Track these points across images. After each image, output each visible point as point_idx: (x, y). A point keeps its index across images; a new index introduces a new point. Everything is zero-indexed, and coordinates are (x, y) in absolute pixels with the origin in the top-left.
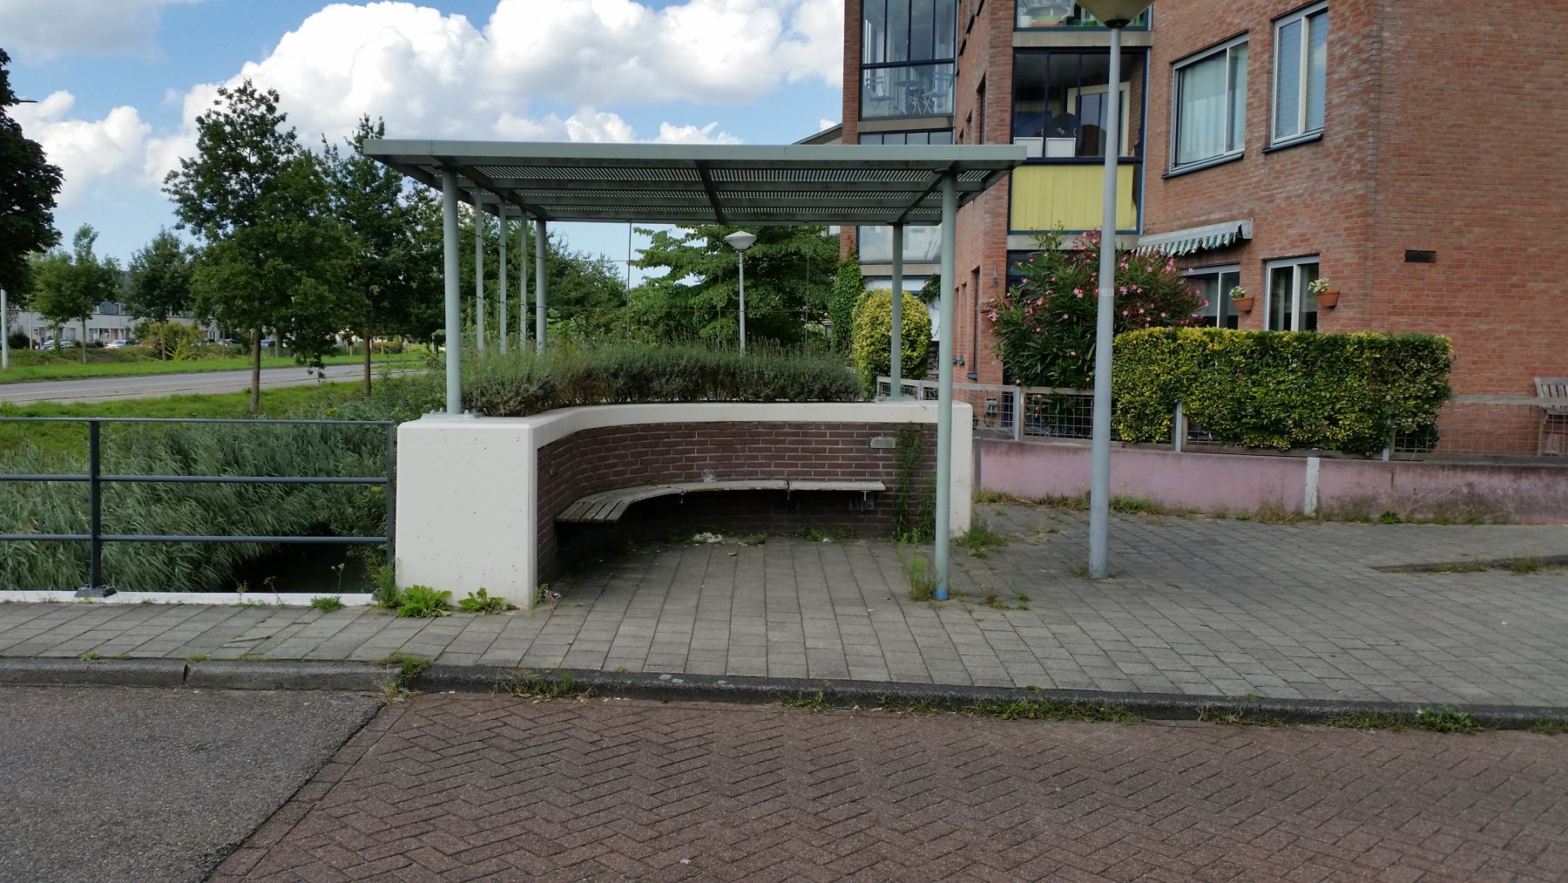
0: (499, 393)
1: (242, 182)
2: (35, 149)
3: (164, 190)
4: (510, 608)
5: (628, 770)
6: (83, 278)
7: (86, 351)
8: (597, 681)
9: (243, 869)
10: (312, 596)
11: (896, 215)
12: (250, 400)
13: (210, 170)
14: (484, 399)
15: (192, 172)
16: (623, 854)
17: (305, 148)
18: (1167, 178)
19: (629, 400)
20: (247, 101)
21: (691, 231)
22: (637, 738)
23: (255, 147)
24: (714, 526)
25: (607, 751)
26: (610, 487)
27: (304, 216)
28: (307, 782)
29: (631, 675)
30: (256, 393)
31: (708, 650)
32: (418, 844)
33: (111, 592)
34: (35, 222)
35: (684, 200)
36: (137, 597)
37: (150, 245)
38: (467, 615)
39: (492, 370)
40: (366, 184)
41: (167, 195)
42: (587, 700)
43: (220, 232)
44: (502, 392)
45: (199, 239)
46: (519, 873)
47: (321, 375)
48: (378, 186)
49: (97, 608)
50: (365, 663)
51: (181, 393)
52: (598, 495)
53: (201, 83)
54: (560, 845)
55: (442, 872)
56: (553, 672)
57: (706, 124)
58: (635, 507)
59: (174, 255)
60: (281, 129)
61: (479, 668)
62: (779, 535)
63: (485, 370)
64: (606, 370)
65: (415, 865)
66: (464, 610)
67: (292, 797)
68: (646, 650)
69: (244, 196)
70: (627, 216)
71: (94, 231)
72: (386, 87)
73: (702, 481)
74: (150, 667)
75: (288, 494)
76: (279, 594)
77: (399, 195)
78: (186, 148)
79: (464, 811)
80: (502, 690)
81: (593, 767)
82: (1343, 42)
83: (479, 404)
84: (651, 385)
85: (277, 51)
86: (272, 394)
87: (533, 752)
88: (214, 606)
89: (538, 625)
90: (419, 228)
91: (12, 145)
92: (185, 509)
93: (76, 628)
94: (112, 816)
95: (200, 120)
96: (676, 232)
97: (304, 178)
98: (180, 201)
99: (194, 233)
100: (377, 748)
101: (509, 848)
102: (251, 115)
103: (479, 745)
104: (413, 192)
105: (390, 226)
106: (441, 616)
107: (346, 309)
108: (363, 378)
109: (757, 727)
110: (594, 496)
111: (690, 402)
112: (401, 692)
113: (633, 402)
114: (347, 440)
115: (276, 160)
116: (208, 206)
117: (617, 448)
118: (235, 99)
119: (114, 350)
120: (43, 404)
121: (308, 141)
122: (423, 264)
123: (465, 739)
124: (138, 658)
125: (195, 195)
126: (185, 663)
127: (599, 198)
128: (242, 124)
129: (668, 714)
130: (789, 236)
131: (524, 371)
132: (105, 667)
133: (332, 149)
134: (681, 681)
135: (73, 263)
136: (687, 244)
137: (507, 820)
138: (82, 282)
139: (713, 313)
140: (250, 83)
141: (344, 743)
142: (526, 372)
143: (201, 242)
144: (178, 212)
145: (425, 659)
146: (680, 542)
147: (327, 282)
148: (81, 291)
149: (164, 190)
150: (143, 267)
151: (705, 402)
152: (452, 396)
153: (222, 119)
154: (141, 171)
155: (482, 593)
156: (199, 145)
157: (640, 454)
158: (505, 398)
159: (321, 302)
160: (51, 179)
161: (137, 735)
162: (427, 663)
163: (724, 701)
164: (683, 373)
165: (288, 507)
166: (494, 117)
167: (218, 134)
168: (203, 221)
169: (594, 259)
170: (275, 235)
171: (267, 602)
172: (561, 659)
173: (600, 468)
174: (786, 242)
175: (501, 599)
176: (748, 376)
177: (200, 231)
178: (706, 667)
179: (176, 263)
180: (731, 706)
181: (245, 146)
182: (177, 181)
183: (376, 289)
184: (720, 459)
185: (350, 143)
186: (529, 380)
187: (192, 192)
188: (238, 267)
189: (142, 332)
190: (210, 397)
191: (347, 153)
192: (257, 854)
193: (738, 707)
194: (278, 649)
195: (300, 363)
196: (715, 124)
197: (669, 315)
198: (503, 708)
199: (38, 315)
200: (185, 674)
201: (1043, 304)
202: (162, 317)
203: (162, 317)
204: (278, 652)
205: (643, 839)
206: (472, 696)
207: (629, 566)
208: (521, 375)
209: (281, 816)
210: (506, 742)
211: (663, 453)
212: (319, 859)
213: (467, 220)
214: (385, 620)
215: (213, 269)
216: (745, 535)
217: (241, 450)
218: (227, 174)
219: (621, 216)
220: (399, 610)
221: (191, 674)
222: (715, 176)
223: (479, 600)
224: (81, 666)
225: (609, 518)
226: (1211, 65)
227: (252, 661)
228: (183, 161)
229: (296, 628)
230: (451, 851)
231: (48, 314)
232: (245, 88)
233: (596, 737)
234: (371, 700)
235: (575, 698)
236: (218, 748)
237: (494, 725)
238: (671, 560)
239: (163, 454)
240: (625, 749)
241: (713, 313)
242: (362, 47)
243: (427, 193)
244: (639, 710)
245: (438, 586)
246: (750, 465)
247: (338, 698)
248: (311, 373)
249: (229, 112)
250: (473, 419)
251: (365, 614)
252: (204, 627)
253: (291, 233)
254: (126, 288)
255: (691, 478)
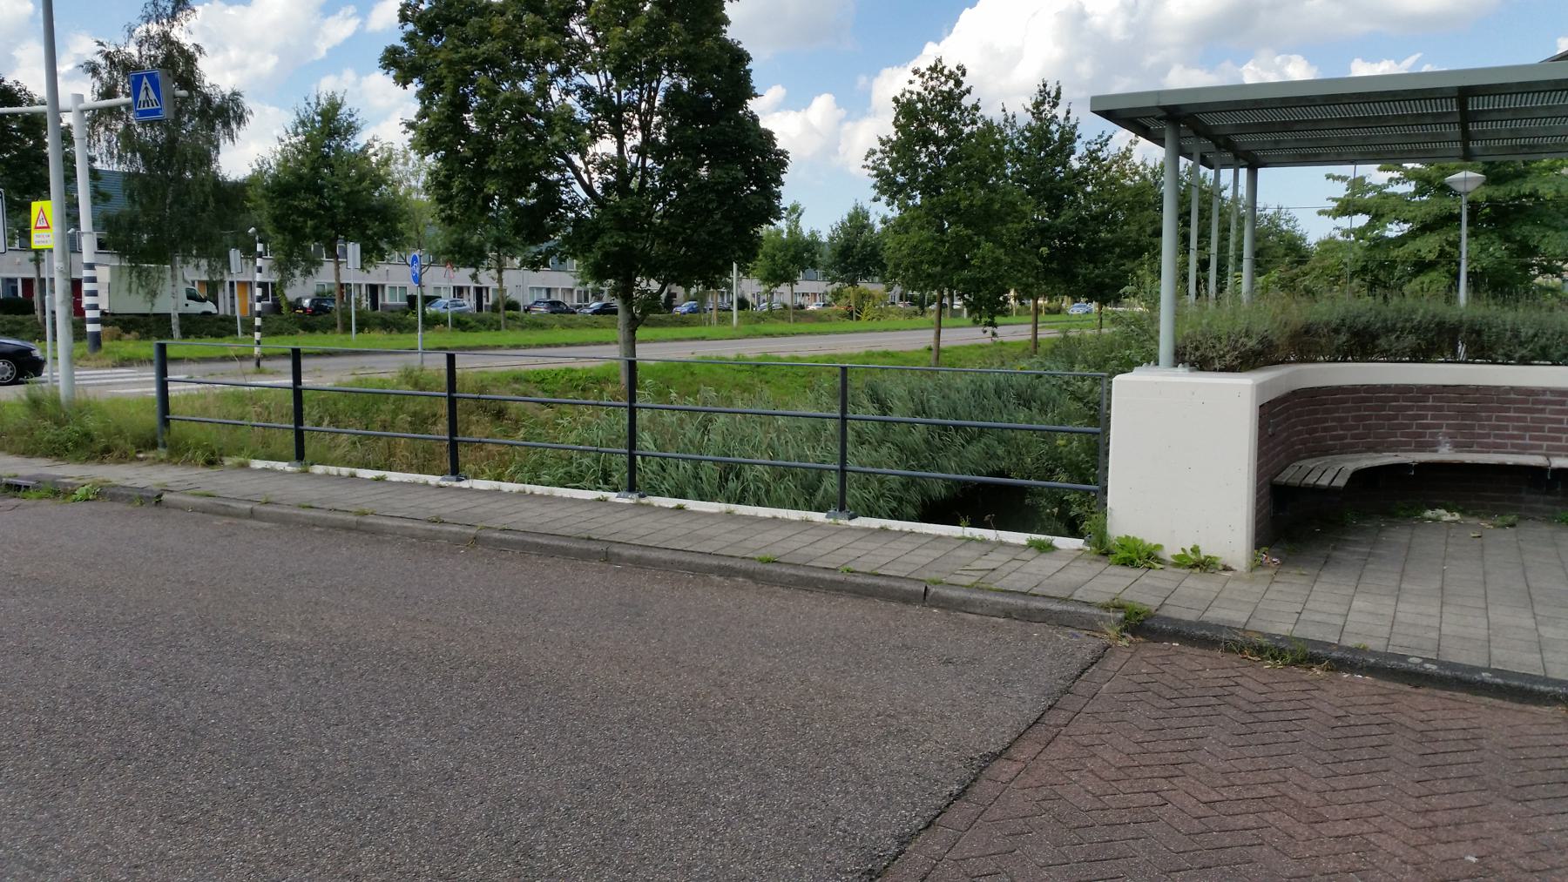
0: (1214, 347)
1: (930, 155)
2: (768, 136)
3: (864, 167)
4: (1226, 569)
5: (1384, 752)
6: (792, 249)
7: (794, 313)
8: (1335, 655)
9: (1004, 778)
10: (1028, 535)
12: (931, 357)
13: (903, 145)
14: (1198, 354)
15: (888, 149)
16: (1394, 836)
17: (988, 118)
19: (1350, 358)
20: (937, 78)
21: (1396, 175)
22: (1387, 720)
23: (944, 121)
24: (1448, 503)
25: (1356, 728)
26: (1326, 452)
27: (984, 184)
28: (1050, 707)
29: (1373, 653)
30: (937, 351)
31: (1464, 638)
32: (1170, 786)
33: (852, 517)
34: (768, 199)
35: (1426, 135)
36: (875, 523)
37: (846, 217)
38: (1180, 570)
39: (1208, 324)
40: (1041, 149)
41: (867, 171)
42: (1324, 673)
43: (910, 202)
44: (1218, 345)
45: (892, 210)
46: (1280, 833)
47: (994, 334)
48: (1052, 150)
49: (844, 530)
50: (1088, 604)
51: (874, 349)
52: (1314, 460)
53: (888, 67)
54: (1319, 814)
55: (1199, 818)
56: (1284, 638)
57: (1407, 57)
58: (1359, 476)
59: (864, 227)
60: (967, 101)
61: (1202, 624)
62: (1533, 519)
63: (1200, 324)
64: (1327, 324)
65: (1169, 805)
66: (1176, 565)
67: (1039, 719)
68: (1387, 629)
69: (931, 168)
70: (1352, 157)
71: (802, 207)
72: (1057, 53)
73: (1436, 451)
74: (896, 584)
75: (968, 443)
76: (998, 532)
77: (1072, 157)
78: (881, 125)
79: (1210, 762)
80: (1228, 650)
81: (1343, 742)
83: (1193, 358)
84: (1377, 342)
85: (955, 30)
86: (949, 351)
87: (1273, 716)
88: (940, 537)
89: (1259, 588)
90: (1089, 189)
91: (753, 134)
92: (884, 450)
93: (829, 545)
94: (886, 709)
95: (896, 100)
96: (1374, 174)
97: (986, 147)
98: (877, 176)
99: (888, 205)
100: (1110, 686)
101: (1265, 807)
102: (941, 91)
103: (1213, 701)
104: (1086, 153)
105: (1062, 188)
106: (1154, 568)
107: (1019, 271)
108: (1030, 337)
109: (1535, 730)
110: (1311, 460)
111: (1422, 362)
112: (1124, 637)
113: (1354, 361)
114: (1019, 396)
115: (961, 132)
116: (900, 179)
117: (1336, 410)
118: (927, 77)
119: (813, 311)
120: (767, 357)
121: (991, 112)
122: (1092, 225)
123: (1196, 692)
124: (884, 575)
125: (891, 169)
126: (924, 584)
127: (1322, 139)
128: (932, 100)
129: (1422, 700)
130: (1520, 175)
131: (1241, 324)
132: (860, 580)
133: (1010, 117)
134: (1434, 667)
135: (785, 236)
136: (1390, 190)
137: (1258, 779)
138: (792, 252)
139: (1422, 267)
140: (940, 61)
141: (1078, 676)
142: (1245, 326)
143: (894, 213)
144: (875, 186)
145: (1146, 608)
146: (1409, 517)
147: (1003, 245)
148: (791, 261)
149: (864, 167)
150: (840, 237)
151: (1442, 362)
152: (1165, 348)
153: (915, 97)
154: (836, 153)
155: (1195, 550)
156: (894, 123)
157: (1364, 418)
158: (1221, 353)
159: (997, 264)
160: (778, 162)
161: (892, 642)
162: (1149, 611)
163: (1490, 697)
164: (1415, 330)
165: (969, 455)
166: (1165, 69)
167: (912, 112)
168: (896, 193)
170: (958, 203)
171: (986, 537)
172: (1291, 627)
173: (1315, 430)
174: (1517, 182)
175: (1216, 558)
176: (1498, 334)
177: (893, 203)
178: (1465, 656)
179: (866, 233)
180: (1498, 702)
181: (933, 122)
182: (875, 158)
183: (1044, 250)
184: (1459, 427)
185: (1028, 110)
186: (1247, 334)
187: (888, 167)
188: (925, 234)
189: (837, 295)
190: (897, 353)
191: (1025, 119)
192: (1016, 767)
193: (1507, 704)
194: (1005, 580)
195: (976, 323)
196: (1418, 55)
197: (1364, 270)
198: (1233, 668)
199: (756, 281)
200: (925, 594)
202: (853, 283)
203: (853, 283)
204: (1004, 584)
205: (1416, 826)
206: (1198, 651)
207: (1350, 538)
208: (1237, 329)
209: (1032, 734)
210: (1241, 703)
211: (1389, 418)
212: (1075, 782)
213: (1137, 178)
214: (1098, 566)
215: (904, 237)
216: (1489, 516)
217: (928, 400)
218: (917, 148)
219: (1345, 158)
220: (1111, 558)
221: (930, 594)
222: (1474, 104)
223: (1193, 557)
224: (839, 577)
225: (1319, 483)
227: (982, 589)
228: (880, 139)
229: (1017, 564)
230: (1205, 799)
231: (765, 280)
232: (936, 66)
233: (1341, 713)
234: (1096, 639)
235: (1310, 668)
236: (963, 663)
237: (1226, 684)
238: (1399, 535)
239: (866, 402)
240: (1376, 730)
241: (1422, 267)
242: (1034, 14)
243: (1100, 154)
244: (1385, 691)
245: (1150, 538)
246: (1496, 436)
247: (1064, 634)
248: (985, 332)
249: (921, 90)
250: (1188, 373)
251: (1078, 558)
252: (936, 554)
253: (972, 201)
254: (825, 257)
255: (1421, 447)
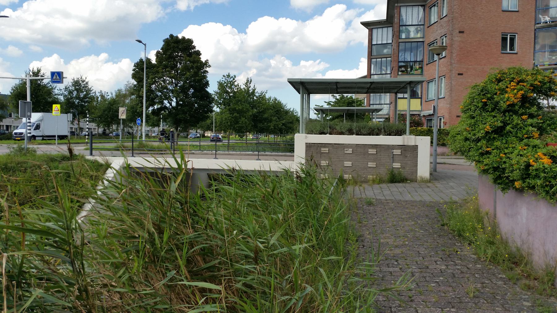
11: (396, 91)
18: (426, 101)
60: (236, 83)
82: (447, 82)
169: (291, 110)
201: (177, 103)
226: (431, 83)
